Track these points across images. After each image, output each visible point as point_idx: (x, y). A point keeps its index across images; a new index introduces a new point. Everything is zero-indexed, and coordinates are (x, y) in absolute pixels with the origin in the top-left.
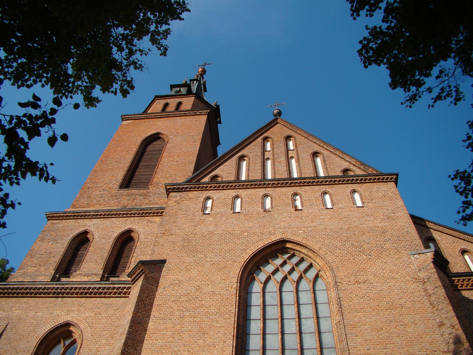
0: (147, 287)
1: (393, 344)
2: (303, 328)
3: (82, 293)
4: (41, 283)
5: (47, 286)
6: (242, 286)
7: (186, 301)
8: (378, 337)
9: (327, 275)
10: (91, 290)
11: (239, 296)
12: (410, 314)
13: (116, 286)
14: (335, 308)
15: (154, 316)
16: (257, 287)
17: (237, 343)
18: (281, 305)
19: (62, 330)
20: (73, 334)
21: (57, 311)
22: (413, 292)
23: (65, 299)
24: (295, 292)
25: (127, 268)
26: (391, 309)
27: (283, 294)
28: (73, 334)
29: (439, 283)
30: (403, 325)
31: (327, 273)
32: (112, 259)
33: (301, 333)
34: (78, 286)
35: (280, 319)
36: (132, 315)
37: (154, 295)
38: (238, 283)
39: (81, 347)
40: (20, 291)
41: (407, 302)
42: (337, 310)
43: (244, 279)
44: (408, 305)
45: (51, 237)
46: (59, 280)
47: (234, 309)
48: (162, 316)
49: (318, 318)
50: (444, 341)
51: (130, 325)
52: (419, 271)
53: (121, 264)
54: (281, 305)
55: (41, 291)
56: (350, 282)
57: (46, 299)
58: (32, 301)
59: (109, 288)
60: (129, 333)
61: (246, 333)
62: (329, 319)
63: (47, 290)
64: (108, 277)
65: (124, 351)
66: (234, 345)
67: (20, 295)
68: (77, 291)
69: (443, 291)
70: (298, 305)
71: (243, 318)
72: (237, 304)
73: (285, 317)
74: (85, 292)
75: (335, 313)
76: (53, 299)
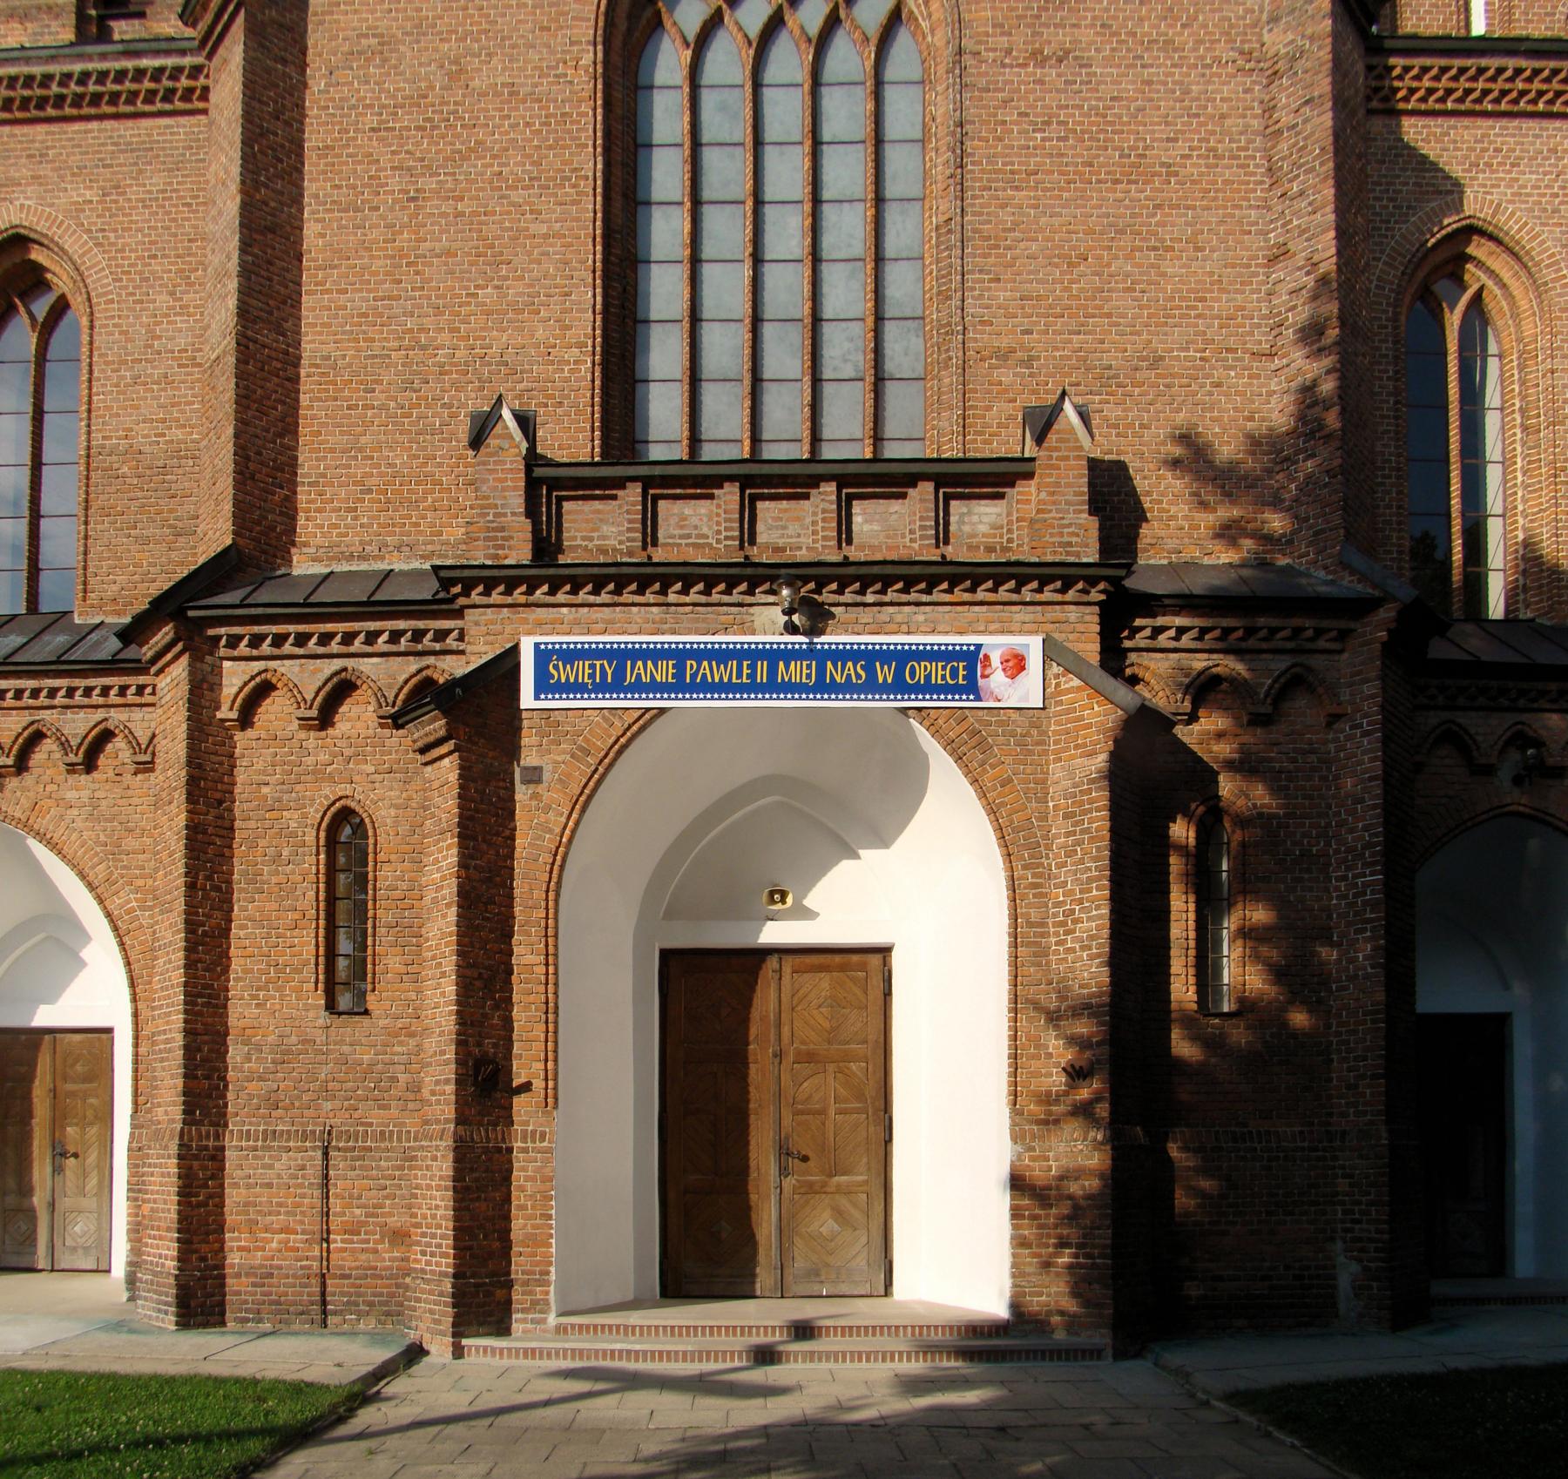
1: (1109, 315)
7: (418, 128)
8: (1065, 289)
10: (55, 88)
12: (1187, 208)
15: (317, 196)
16: (669, 63)
20: (49, 276)
22: (1223, 116)
24: (807, 87)
26: (1129, 182)
27: (767, 93)
29: (1324, 85)
30: (1155, 249)
33: (816, 258)
35: (750, 203)
36: (238, 199)
37: (300, 106)
38: (600, 47)
39: (92, 327)
41: (1189, 157)
42: (948, 172)
43: (622, 25)
44: (1191, 169)
47: (591, 164)
49: (879, 200)
50: (1271, 315)
52: (1274, 20)
56: (1008, 52)
59: (121, 76)
60: (245, 272)
61: (636, 255)
62: (918, 205)
64: (102, 20)
65: (244, 341)
66: (598, 307)
69: (1327, 120)
71: (625, 195)
72: (599, 142)
73: (769, 195)
75: (941, 186)
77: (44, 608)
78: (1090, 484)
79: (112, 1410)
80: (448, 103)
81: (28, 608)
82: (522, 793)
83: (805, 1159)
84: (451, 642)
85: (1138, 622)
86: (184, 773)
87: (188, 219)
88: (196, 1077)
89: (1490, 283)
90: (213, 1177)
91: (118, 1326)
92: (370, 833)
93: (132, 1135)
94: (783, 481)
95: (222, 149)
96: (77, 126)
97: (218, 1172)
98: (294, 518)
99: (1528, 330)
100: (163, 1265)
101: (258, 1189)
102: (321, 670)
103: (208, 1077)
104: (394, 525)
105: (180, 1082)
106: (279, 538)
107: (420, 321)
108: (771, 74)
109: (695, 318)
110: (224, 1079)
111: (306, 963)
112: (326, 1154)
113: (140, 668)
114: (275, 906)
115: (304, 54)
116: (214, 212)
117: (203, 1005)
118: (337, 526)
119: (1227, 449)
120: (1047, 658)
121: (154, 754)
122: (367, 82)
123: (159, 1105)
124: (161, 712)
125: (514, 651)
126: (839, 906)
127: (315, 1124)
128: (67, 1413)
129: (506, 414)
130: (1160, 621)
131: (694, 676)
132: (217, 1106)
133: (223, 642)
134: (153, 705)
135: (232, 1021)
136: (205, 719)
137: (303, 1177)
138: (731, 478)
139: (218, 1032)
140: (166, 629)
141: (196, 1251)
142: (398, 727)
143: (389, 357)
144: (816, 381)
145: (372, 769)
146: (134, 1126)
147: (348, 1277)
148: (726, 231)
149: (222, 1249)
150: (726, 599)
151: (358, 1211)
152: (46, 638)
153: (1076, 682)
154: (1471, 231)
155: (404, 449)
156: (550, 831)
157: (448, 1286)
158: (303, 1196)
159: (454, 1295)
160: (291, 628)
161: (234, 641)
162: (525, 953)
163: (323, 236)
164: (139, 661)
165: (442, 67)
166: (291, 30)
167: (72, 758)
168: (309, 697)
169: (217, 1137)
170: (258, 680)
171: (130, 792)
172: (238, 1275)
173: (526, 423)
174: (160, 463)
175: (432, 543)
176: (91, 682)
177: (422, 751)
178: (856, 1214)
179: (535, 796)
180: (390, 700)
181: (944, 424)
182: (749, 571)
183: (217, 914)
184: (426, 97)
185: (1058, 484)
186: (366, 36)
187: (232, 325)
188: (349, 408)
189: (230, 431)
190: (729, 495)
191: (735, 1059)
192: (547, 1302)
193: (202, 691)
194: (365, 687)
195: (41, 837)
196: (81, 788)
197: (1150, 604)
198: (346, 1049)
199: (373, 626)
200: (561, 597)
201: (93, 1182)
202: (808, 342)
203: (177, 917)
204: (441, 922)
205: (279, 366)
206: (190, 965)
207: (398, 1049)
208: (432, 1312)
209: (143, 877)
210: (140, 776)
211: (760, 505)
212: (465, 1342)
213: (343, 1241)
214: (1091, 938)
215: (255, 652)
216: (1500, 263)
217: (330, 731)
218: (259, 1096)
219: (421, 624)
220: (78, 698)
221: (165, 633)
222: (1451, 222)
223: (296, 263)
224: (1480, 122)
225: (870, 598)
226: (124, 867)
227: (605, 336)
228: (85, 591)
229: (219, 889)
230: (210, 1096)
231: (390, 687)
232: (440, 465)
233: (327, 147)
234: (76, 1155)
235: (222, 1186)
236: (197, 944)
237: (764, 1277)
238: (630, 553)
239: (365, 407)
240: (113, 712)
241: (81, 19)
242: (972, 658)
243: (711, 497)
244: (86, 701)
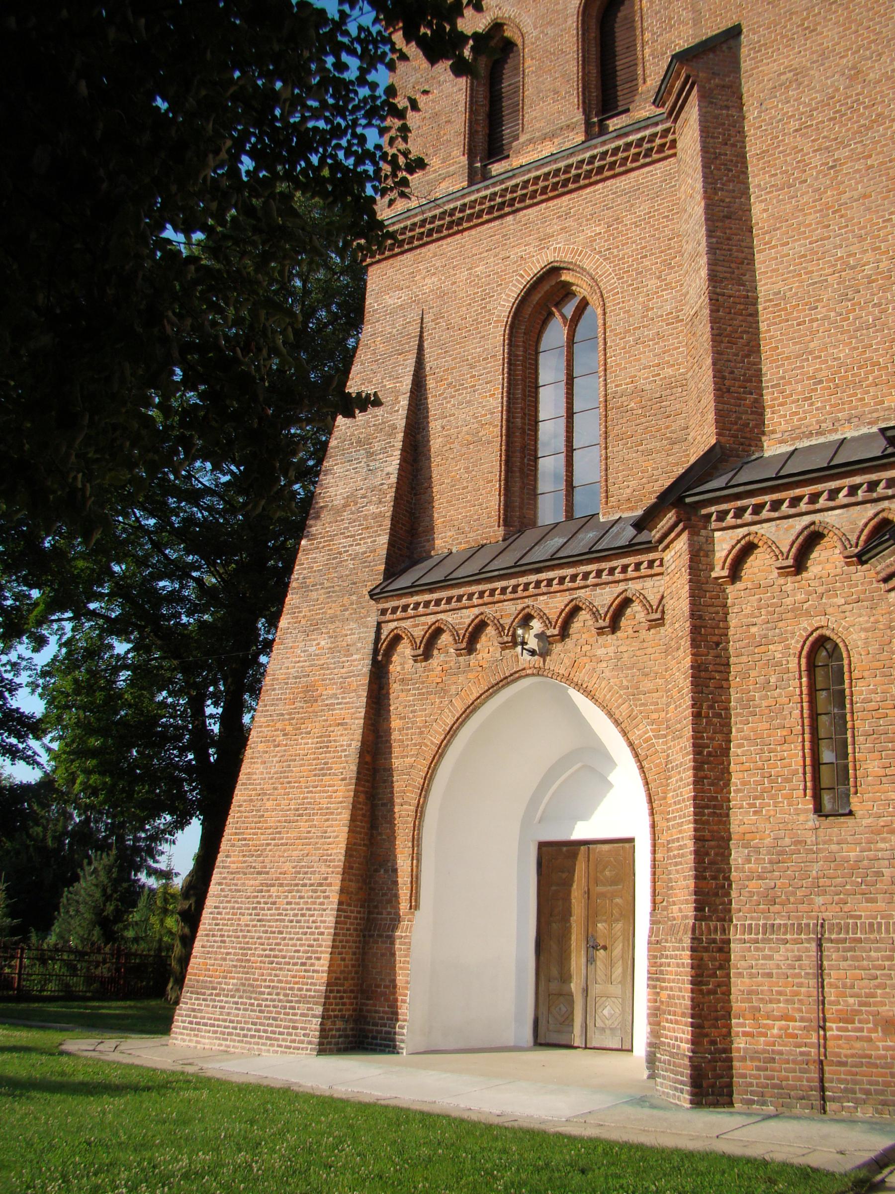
0: (716, 117)
3: (555, 186)
4: (451, 196)
5: (466, 200)
7: (830, 120)
13: (631, 138)
15: (759, 185)
19: (546, 287)
20: (574, 288)
21: (516, 250)
23: (522, 213)
25: (640, 81)
28: (574, 288)
32: (594, 70)
34: (538, 173)
36: (703, 204)
37: (741, 132)
39: (604, 314)
40: (411, 234)
45: (418, 75)
46: (485, 176)
48: (779, 180)
51: (707, 230)
53: (621, 76)
55: (458, 215)
57: (479, 229)
58: (450, 246)
59: (616, 151)
60: (712, 250)
63: (471, 208)
65: (715, 297)
67: (416, 243)
68: (541, 184)
74: (560, 182)
76: (493, 224)
77: (577, 515)
79: (642, 1179)
80: (851, 96)
81: (567, 517)
86: (688, 624)
87: (667, 226)
88: (705, 878)
90: (721, 967)
91: (641, 1101)
92: (845, 655)
93: (651, 930)
95: (688, 175)
97: (725, 964)
98: (762, 414)
100: (679, 1047)
101: (760, 979)
102: (792, 527)
103: (715, 878)
104: (843, 404)
105: (691, 883)
106: (752, 431)
107: (848, 249)
110: (728, 878)
111: (795, 772)
112: (820, 946)
113: (650, 547)
114: (766, 725)
115: (741, 99)
116: (686, 216)
117: (709, 815)
118: (797, 413)
121: (663, 612)
122: (788, 102)
123: (674, 903)
124: (668, 580)
127: (809, 917)
128: (606, 1177)
132: (723, 903)
133: (714, 517)
134: (662, 574)
135: (734, 828)
136: (703, 579)
137: (800, 967)
139: (723, 838)
140: (670, 515)
141: (707, 1035)
142: (863, 563)
143: (826, 280)
145: (843, 601)
146: (653, 922)
147: (844, 1064)
149: (729, 1033)
151: (851, 1000)
152: (580, 536)
155: (845, 345)
158: (800, 985)
160: (767, 498)
161: (722, 516)
163: (766, 210)
164: (650, 542)
165: (843, 74)
166: (731, 87)
167: (601, 623)
168: (785, 550)
169: (724, 931)
170: (743, 542)
171: (645, 645)
172: (743, 1059)
174: (658, 395)
175: (876, 411)
176: (614, 563)
177: (886, 580)
180: (853, 542)
183: (718, 736)
184: (833, 97)
186: (784, 73)
187: (705, 288)
188: (798, 325)
189: (709, 361)
193: (699, 558)
194: (831, 534)
195: (579, 687)
196: (609, 645)
198: (834, 847)
199: (833, 485)
201: (618, 971)
203: (686, 742)
205: (742, 307)
206: (698, 781)
207: (881, 845)
209: (656, 711)
210: (652, 631)
213: (838, 1029)
215: (739, 521)
217: (804, 575)
218: (758, 893)
219: (874, 477)
220: (605, 577)
221: (670, 517)
223: (748, 234)
226: (642, 705)
228: (607, 497)
229: (719, 715)
230: (717, 895)
231: (852, 531)
232: (877, 350)
233: (763, 152)
234: (605, 948)
235: (728, 976)
236: (703, 763)
240: (631, 584)
241: (588, 125)
244: (610, 578)
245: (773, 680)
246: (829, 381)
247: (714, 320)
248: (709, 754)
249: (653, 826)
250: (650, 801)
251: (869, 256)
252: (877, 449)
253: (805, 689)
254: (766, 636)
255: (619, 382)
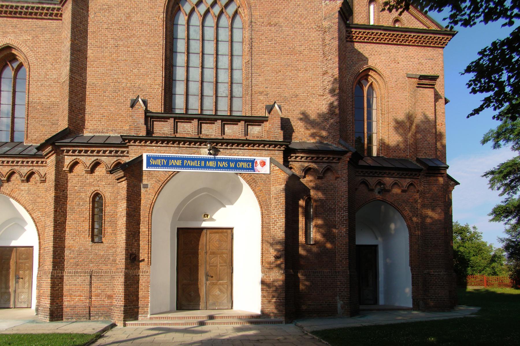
0: (78, 11)
2: (220, 64)
6: (169, 17)
7: (118, 29)
9: (244, 12)
11: (166, 28)
14: (247, 48)
15: (91, 44)
16: (182, 19)
17: (165, 73)
18: (203, 40)
22: (313, 41)
24: (215, 27)
27: (205, 28)
29: (336, 35)
31: (245, 11)
35: (201, 54)
37: (87, 21)
39: (29, 71)
43: (170, 9)
44: (305, 52)
48: (98, 44)
52: (325, 19)
54: (203, 40)
56: (263, 23)
59: (38, 8)
60: (72, 61)
69: (337, 43)
70: (217, 41)
71: (170, 50)
75: (247, 53)
77: (15, 141)
78: (281, 123)
82: (143, 190)
83: (212, 277)
84: (125, 154)
85: (292, 155)
89: (374, 81)
90: (60, 283)
91: (33, 321)
93: (38, 273)
94: (208, 119)
96: (25, 20)
98: (84, 122)
99: (383, 92)
103: (59, 258)
105: (52, 260)
106: (80, 126)
108: (207, 23)
109: (187, 80)
110: (64, 259)
111: (86, 230)
112: (91, 277)
113: (42, 157)
116: (63, 45)
118: (96, 124)
119: (313, 116)
120: (271, 162)
124: (48, 167)
125: (142, 156)
126: (220, 218)
129: (140, 100)
130: (297, 155)
131: (186, 164)
135: (66, 244)
138: (196, 118)
142: (111, 174)
144: (217, 97)
146: (39, 271)
148: (195, 60)
149: (62, 301)
150: (194, 146)
152: (16, 148)
153: (278, 168)
154: (370, 69)
156: (150, 199)
157: (122, 309)
158: (85, 287)
159: (124, 311)
160: (83, 149)
161: (68, 151)
162: (143, 228)
167: (23, 179)
168: (88, 166)
169: (62, 273)
172: (67, 307)
173: (145, 102)
177: (118, 180)
178: (224, 290)
179: (146, 191)
181: (247, 108)
182: (200, 140)
185: (273, 123)
189: (68, 100)
190: (195, 122)
191: (195, 254)
192: (148, 312)
193: (59, 164)
195: (14, 198)
196: (25, 186)
197: (295, 151)
198: (96, 251)
200: (153, 144)
201: (27, 285)
202: (215, 87)
203: (51, 218)
204: (122, 221)
206: (55, 231)
208: (118, 315)
211: (203, 125)
212: (126, 322)
214: (281, 226)
216: (376, 76)
217: (93, 174)
219: (117, 149)
220: (25, 164)
221: (49, 149)
222: (365, 67)
224: (372, 45)
225: (229, 147)
227: (165, 83)
231: (109, 164)
234: (22, 278)
235: (63, 285)
237: (202, 305)
238: (171, 135)
239: (104, 96)
242: (253, 162)
243: (191, 122)
244: (27, 164)
245: (81, 203)
246: (107, 117)
247: (71, 86)
248: (59, 223)
249: (40, 243)
250: (39, 235)
251: (124, 81)
252: (119, 141)
253: (91, 207)
254: (80, 190)
255: (34, 98)
